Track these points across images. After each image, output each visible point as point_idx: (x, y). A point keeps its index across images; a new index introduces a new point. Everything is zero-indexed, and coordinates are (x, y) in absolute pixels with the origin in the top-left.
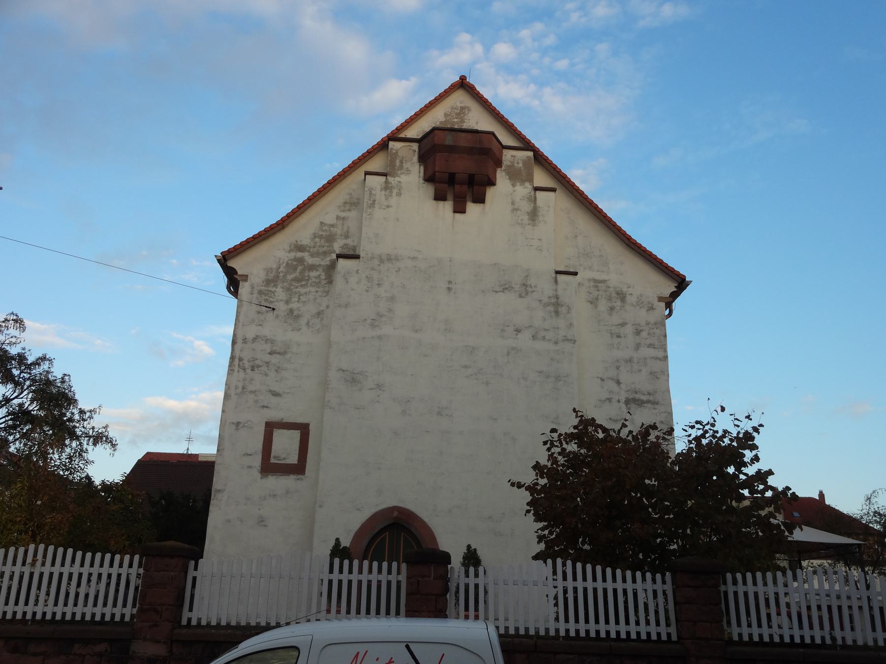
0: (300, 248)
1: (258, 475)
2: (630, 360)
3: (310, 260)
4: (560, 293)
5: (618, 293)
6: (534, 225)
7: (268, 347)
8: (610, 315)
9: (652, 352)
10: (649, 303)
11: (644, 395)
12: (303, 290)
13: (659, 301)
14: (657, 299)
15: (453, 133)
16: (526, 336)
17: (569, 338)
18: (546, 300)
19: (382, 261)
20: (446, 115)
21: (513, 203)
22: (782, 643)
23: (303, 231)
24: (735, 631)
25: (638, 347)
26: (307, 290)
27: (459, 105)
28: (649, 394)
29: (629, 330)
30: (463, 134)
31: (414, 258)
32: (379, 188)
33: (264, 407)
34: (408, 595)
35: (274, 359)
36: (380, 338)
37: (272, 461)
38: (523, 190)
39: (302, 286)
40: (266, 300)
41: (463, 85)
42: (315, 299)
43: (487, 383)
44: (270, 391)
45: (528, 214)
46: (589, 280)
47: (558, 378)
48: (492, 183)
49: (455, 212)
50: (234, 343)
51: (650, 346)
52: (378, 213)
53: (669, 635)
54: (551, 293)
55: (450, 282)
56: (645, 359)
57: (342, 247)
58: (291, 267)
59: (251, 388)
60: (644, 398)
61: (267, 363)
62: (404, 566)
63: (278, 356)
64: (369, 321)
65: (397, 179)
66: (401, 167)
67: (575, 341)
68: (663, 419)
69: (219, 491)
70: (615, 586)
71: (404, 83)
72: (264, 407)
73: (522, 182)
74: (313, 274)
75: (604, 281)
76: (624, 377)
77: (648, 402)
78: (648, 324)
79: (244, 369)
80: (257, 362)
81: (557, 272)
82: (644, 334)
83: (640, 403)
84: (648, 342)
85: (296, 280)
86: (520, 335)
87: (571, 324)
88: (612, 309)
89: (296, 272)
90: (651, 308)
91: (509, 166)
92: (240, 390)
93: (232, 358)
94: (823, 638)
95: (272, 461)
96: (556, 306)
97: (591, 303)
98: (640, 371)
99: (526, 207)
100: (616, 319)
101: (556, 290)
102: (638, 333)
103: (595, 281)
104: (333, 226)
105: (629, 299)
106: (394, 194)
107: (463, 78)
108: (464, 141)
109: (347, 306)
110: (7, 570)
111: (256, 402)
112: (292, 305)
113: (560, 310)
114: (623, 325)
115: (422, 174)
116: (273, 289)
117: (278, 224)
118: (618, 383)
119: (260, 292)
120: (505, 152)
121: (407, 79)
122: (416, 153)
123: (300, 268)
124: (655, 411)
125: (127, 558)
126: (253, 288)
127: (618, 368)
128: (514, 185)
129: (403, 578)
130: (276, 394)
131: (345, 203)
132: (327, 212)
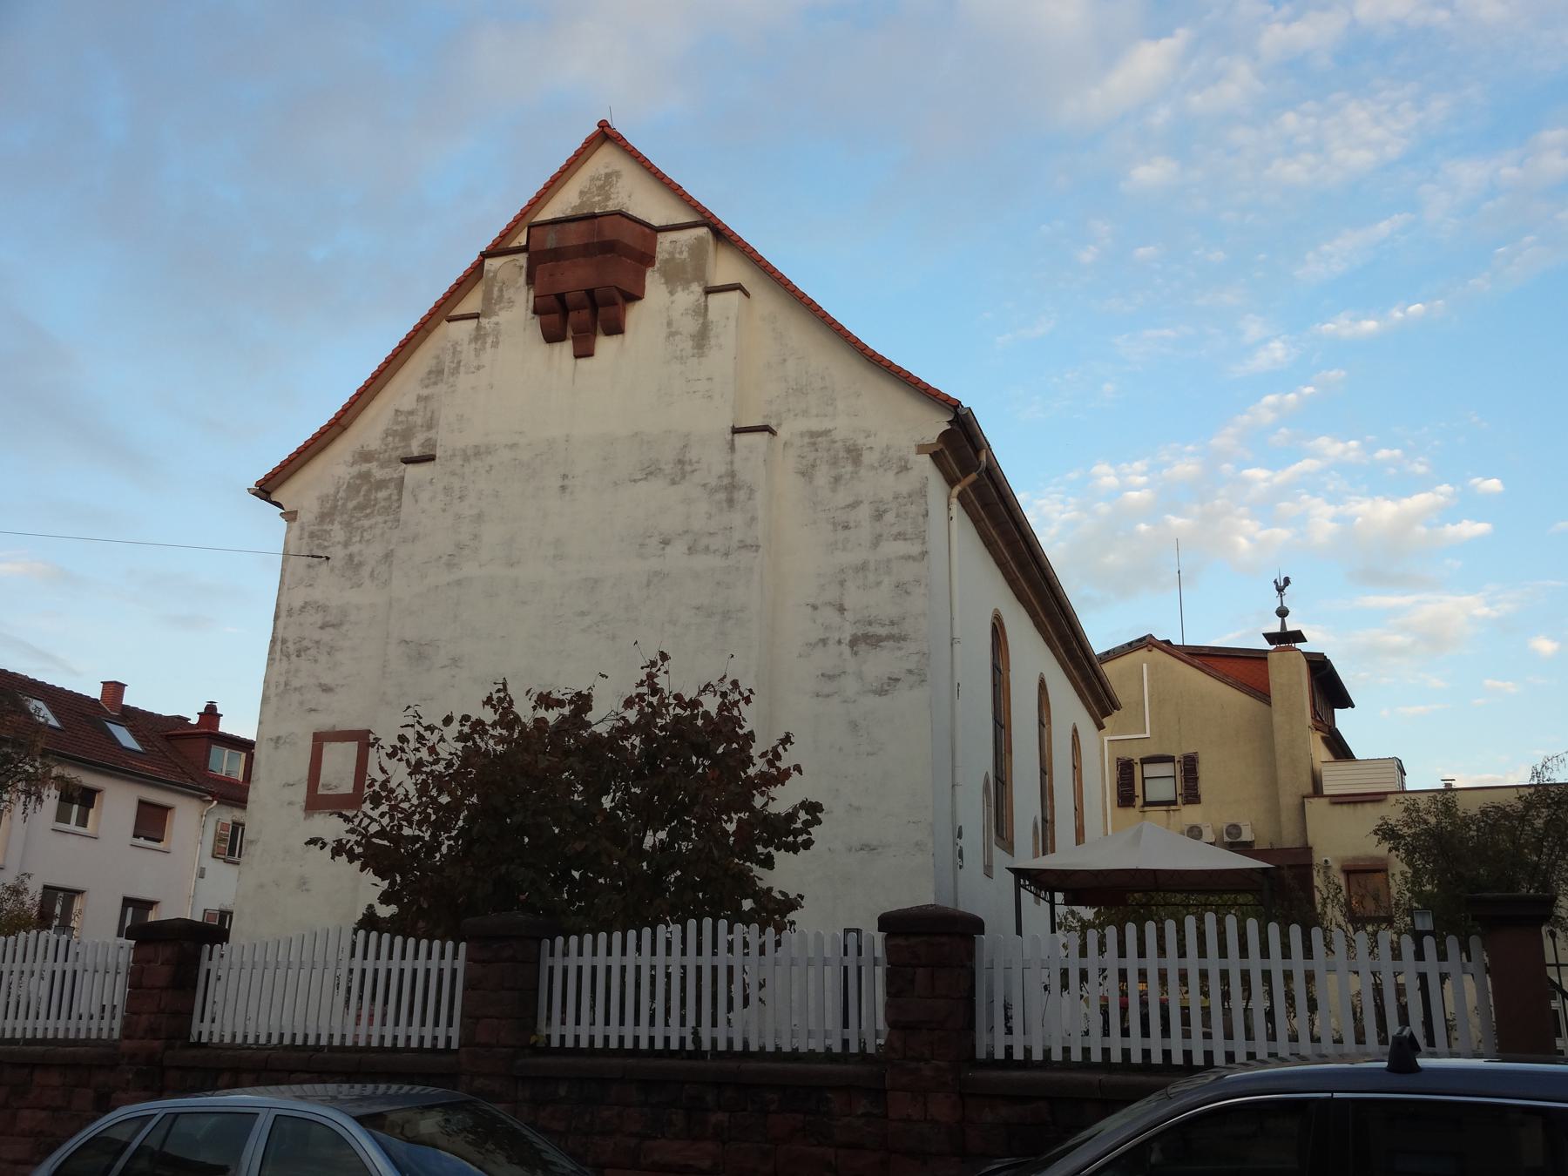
0: (366, 456)
1: (301, 814)
2: (863, 567)
3: (379, 473)
4: (737, 466)
5: (849, 451)
6: (701, 356)
7: (318, 618)
8: (834, 490)
9: (901, 547)
10: (900, 459)
11: (884, 626)
12: (366, 523)
13: (919, 452)
14: (914, 449)
15: (558, 227)
16: (678, 548)
17: (749, 542)
18: (713, 482)
19: (466, 459)
20: (582, 193)
21: (669, 324)
22: (1027, 1063)
23: (370, 430)
24: (555, 1032)
25: (877, 540)
26: (373, 521)
27: (603, 171)
28: (892, 623)
29: (864, 512)
30: (573, 226)
31: (513, 446)
32: (466, 339)
33: (312, 710)
34: (465, 989)
35: (326, 636)
36: (459, 583)
37: (321, 791)
38: (688, 296)
39: (367, 516)
40: (319, 546)
41: (605, 135)
42: (383, 534)
43: (614, 638)
44: (320, 685)
45: (693, 337)
46: (802, 435)
47: (726, 615)
48: (634, 296)
49: (577, 357)
50: (276, 617)
51: (900, 536)
52: (464, 380)
53: (449, 1039)
54: (722, 469)
55: (565, 476)
56: (889, 561)
57: (422, 445)
58: (353, 489)
59: (296, 683)
60: (883, 631)
61: (317, 642)
62: (1475, 942)
63: (331, 630)
64: (445, 558)
65: (494, 319)
66: (501, 296)
67: (758, 547)
68: (912, 666)
69: (252, 842)
70: (1246, 964)
71: (1167, 44)
72: (312, 710)
73: (687, 283)
74: (382, 494)
75: (826, 433)
76: (854, 598)
77: (890, 637)
78: (896, 498)
79: (288, 656)
80: (305, 643)
81: (736, 431)
82: (890, 517)
83: (874, 641)
84: (895, 530)
85: (360, 507)
86: (668, 549)
87: (753, 519)
88: (837, 479)
89: (369, 497)
90: (904, 468)
91: (667, 261)
92: (282, 687)
93: (273, 641)
94: (682, 1040)
95: (321, 791)
96: (730, 489)
97: (803, 474)
98: (879, 584)
99: (690, 325)
100: (843, 497)
101: (732, 463)
102: (879, 516)
103: (813, 434)
104: (411, 413)
105: (868, 458)
106: (488, 345)
107: (603, 125)
108: (574, 236)
109: (415, 538)
110: (5, 968)
111: (301, 703)
112: (354, 549)
113: (736, 496)
114: (854, 505)
115: (531, 304)
116: (328, 527)
117: (331, 424)
118: (841, 609)
119: (312, 535)
120: (661, 237)
121: (1170, 34)
122: (524, 272)
123: (364, 488)
124: (899, 654)
125: (437, 944)
126: (302, 529)
127: (842, 583)
128: (672, 293)
129: (460, 964)
130: (327, 689)
131: (430, 372)
132: (403, 392)
